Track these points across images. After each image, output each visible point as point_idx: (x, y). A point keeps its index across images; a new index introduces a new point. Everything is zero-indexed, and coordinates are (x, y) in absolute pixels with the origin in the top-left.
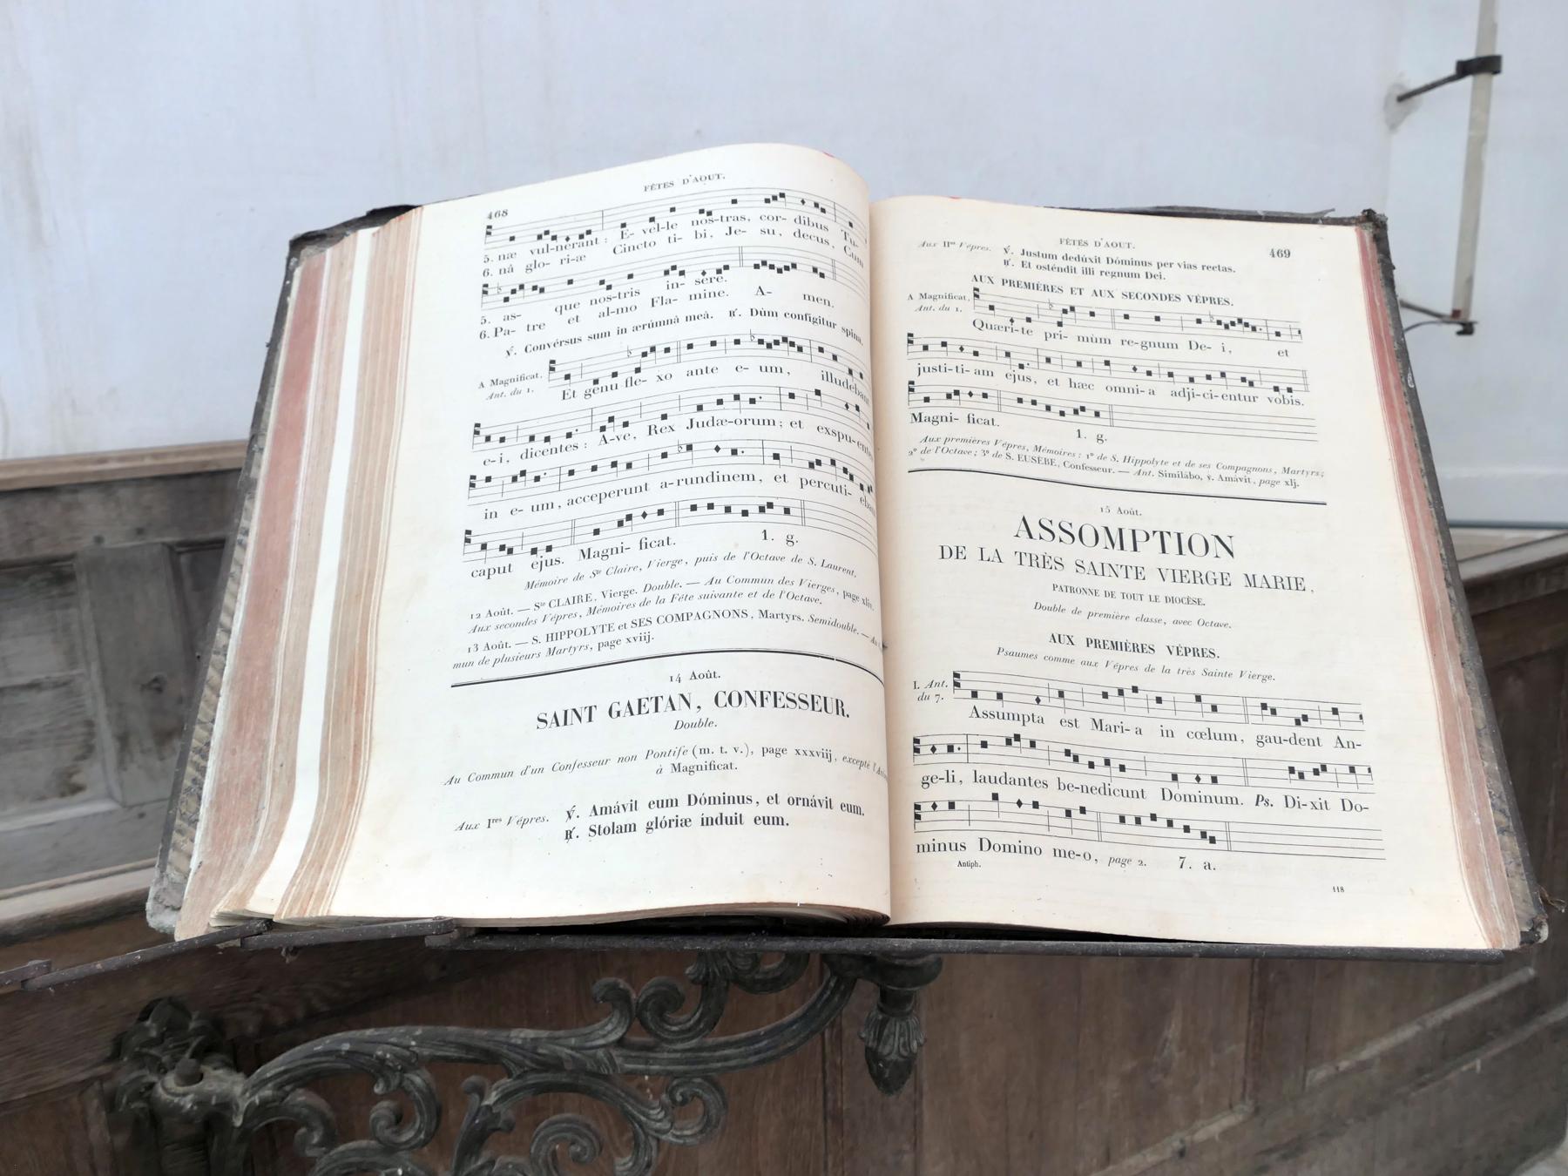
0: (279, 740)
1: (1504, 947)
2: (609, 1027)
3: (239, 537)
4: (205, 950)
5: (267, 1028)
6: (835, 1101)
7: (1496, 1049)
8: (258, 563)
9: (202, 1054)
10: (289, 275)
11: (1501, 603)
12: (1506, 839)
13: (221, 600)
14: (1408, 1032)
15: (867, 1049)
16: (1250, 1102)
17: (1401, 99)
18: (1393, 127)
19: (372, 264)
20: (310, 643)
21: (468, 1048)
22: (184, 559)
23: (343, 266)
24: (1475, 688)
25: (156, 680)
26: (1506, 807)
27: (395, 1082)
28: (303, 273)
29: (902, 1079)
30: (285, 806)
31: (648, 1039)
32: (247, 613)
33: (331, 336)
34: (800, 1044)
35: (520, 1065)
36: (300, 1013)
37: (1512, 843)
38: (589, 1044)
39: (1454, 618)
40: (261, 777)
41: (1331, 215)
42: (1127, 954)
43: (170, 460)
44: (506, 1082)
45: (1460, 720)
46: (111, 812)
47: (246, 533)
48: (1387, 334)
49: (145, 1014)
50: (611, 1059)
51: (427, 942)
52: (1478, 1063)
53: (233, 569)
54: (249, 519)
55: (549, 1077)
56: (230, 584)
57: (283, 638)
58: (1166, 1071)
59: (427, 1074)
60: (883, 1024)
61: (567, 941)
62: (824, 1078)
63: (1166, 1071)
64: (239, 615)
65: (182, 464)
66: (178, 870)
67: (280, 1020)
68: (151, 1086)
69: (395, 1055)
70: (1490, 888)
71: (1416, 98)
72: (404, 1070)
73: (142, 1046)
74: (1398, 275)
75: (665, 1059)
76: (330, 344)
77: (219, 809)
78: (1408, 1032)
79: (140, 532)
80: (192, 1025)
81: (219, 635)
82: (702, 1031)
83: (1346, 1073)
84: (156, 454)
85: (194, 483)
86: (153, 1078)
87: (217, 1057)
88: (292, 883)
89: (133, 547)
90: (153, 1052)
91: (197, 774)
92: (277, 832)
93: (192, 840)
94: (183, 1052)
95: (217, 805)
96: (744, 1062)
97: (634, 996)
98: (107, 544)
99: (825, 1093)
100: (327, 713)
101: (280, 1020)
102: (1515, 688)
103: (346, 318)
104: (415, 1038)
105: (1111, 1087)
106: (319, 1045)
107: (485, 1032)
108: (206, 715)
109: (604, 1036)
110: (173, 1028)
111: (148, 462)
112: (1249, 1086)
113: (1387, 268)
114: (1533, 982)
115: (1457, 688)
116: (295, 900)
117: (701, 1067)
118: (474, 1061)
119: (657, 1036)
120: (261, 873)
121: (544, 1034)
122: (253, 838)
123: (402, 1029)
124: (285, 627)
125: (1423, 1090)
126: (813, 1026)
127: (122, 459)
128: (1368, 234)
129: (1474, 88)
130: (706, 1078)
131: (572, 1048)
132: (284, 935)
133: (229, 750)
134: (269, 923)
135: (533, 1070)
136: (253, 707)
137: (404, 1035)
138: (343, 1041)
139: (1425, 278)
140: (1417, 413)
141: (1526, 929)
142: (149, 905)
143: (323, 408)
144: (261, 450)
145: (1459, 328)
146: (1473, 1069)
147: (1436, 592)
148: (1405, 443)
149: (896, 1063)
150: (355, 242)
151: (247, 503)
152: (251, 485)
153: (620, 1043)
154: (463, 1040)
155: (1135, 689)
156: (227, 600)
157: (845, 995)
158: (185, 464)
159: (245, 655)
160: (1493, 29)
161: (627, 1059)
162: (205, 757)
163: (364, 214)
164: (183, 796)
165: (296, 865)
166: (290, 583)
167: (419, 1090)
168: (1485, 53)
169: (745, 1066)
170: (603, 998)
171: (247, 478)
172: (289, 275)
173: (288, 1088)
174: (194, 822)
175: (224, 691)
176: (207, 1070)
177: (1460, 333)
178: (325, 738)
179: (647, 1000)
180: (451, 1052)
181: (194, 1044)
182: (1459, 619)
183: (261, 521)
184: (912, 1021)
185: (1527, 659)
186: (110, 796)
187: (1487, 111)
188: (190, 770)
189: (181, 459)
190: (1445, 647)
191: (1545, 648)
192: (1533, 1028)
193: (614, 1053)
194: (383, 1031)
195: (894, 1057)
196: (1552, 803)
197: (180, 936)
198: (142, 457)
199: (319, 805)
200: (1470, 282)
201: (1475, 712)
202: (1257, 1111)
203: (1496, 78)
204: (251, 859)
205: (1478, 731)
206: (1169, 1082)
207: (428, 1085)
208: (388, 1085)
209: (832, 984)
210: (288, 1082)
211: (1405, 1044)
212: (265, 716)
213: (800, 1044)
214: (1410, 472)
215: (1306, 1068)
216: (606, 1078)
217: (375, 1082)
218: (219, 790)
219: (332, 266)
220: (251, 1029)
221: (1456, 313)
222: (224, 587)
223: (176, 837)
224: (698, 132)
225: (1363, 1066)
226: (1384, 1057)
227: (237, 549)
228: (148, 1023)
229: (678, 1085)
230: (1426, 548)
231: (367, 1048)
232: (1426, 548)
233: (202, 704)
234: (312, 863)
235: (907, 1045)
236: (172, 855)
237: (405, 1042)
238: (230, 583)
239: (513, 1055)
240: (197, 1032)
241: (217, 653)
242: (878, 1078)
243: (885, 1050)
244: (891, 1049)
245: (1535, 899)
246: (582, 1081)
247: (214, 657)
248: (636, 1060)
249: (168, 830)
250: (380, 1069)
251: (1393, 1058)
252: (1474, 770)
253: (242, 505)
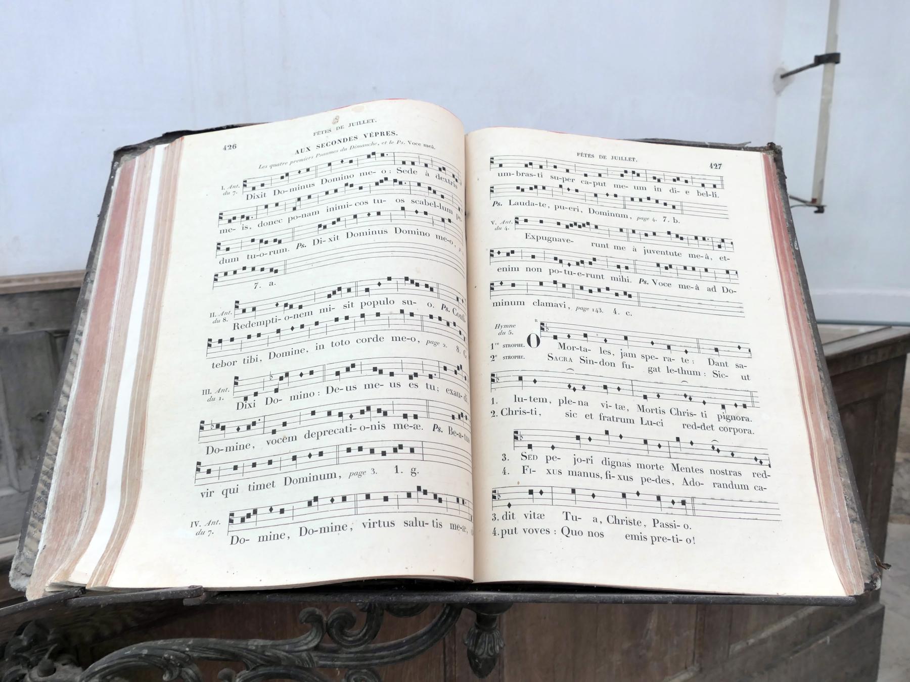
0: (96, 467)
1: (855, 594)
2: (310, 638)
3: (77, 336)
4: (43, 604)
5: (98, 638)
6: (451, 671)
7: (838, 630)
8: (88, 354)
9: (55, 656)
10: (113, 173)
11: (842, 371)
12: (855, 526)
13: (64, 377)
15: (469, 651)
16: (697, 665)
17: (783, 77)
18: (778, 92)
19: (164, 167)
20: (118, 405)
21: (222, 652)
22: (58, 341)
23: (145, 168)
24: (836, 432)
25: (40, 415)
26: (855, 506)
27: (176, 673)
28: (122, 172)
29: (490, 669)
30: (99, 511)
31: (333, 645)
32: (80, 385)
33: (137, 211)
34: (427, 648)
35: (254, 662)
36: (119, 628)
37: (858, 527)
38: (297, 649)
39: (823, 390)
40: (84, 491)
41: (749, 145)
42: (628, 602)
43: (50, 281)
44: (245, 673)
45: (827, 453)
46: (11, 496)
47: (81, 334)
48: (782, 217)
49: (20, 631)
50: (311, 659)
51: (185, 602)
52: (828, 639)
53: (72, 356)
54: (83, 325)
55: (272, 669)
56: (70, 367)
57: (101, 402)
58: (648, 648)
59: (196, 668)
60: (478, 636)
61: (277, 598)
62: (445, 658)
63: (648, 648)
64: (75, 386)
65: (57, 283)
66: (31, 550)
67: (106, 633)
68: (24, 675)
69: (176, 656)
70: (846, 556)
71: (791, 77)
72: (181, 666)
73: (17, 651)
74: (788, 182)
75: (345, 657)
76: (136, 216)
77: (57, 511)
79: (31, 324)
80: (50, 638)
81: (62, 398)
82: (366, 641)
83: (753, 645)
84: (42, 277)
86: (26, 671)
87: (66, 657)
88: (100, 563)
89: (27, 334)
90: (24, 655)
91: (45, 488)
92: (93, 527)
93: (40, 531)
94: (44, 654)
95: (57, 509)
96: (393, 659)
97: (325, 619)
98: (11, 331)
99: (445, 666)
100: (127, 450)
101: (106, 633)
102: (851, 419)
103: (146, 200)
104: (189, 646)
105: (616, 658)
106: (128, 651)
107: (231, 642)
108: (52, 450)
109: (306, 644)
110: (37, 641)
111: (37, 282)
112: (697, 656)
113: (782, 177)
115: (826, 433)
116: (100, 575)
117: (366, 663)
118: (226, 660)
119: (338, 643)
120: (80, 556)
121: (269, 643)
122: (78, 531)
123: (181, 640)
124: (102, 395)
125: (797, 655)
126: (436, 637)
127: (20, 280)
128: (771, 158)
129: (825, 71)
130: (370, 670)
131: (287, 652)
132: (92, 598)
133: (65, 473)
134: (83, 590)
135: (262, 665)
136: (82, 444)
137: (182, 644)
138: (142, 648)
139: (800, 184)
140: (800, 265)
141: (868, 582)
142: (11, 573)
143: (131, 256)
144: (92, 282)
145: (816, 209)
146: (825, 642)
147: (812, 374)
148: (793, 283)
149: (486, 660)
150: (154, 153)
151: (82, 315)
152: (86, 303)
153: (316, 648)
154: (218, 647)
155: (608, 289)
156: (68, 376)
157: (455, 618)
158: (59, 283)
159: (77, 413)
160: (836, 38)
161: (320, 657)
162: (50, 477)
164: (35, 502)
165: (104, 549)
166: (107, 366)
167: (191, 678)
168: (831, 51)
169: (394, 662)
170: (306, 621)
171: (83, 299)
172: (113, 173)
173: (109, 677)
174: (42, 519)
175: (63, 435)
176: (58, 665)
177: (816, 212)
178: (125, 467)
179: (333, 622)
180: (212, 655)
181: (52, 648)
182: (826, 391)
183: (91, 326)
184: (496, 634)
185: (856, 403)
186: (11, 485)
187: (832, 84)
188: (40, 485)
189: (57, 281)
190: (818, 407)
191: (866, 396)
192: (859, 617)
193: (313, 654)
194: (169, 642)
195: (485, 656)
196: (870, 486)
197: (31, 596)
198: (33, 279)
199: (120, 510)
200: (822, 182)
201: (835, 448)
202: (701, 670)
203: (837, 66)
204: (75, 546)
205: (838, 459)
206: (650, 654)
207: (196, 675)
208: (171, 674)
209: (447, 611)
210: (109, 674)
211: (786, 628)
212: (88, 451)
213: (427, 648)
214: (796, 301)
215: (730, 644)
216: (308, 670)
217: (163, 673)
218: (59, 499)
219: (139, 168)
220: (88, 639)
221: (814, 201)
222: (66, 368)
223: (30, 529)
224: (374, 88)
225: (763, 642)
226: (774, 636)
227: (75, 344)
228: (22, 637)
229: (352, 674)
230: (806, 347)
231: (158, 652)
232: (806, 347)
233: (50, 443)
234: (114, 548)
235: (493, 648)
236: (27, 540)
237: (183, 649)
238: (69, 365)
239: (250, 656)
240: (53, 641)
241: (60, 410)
242: (475, 669)
243: (479, 652)
244: (482, 652)
245: (873, 563)
246: (293, 671)
247: (58, 413)
248: (326, 658)
249: (25, 524)
250: (167, 665)
251: (781, 636)
252: (836, 483)
253: (79, 316)
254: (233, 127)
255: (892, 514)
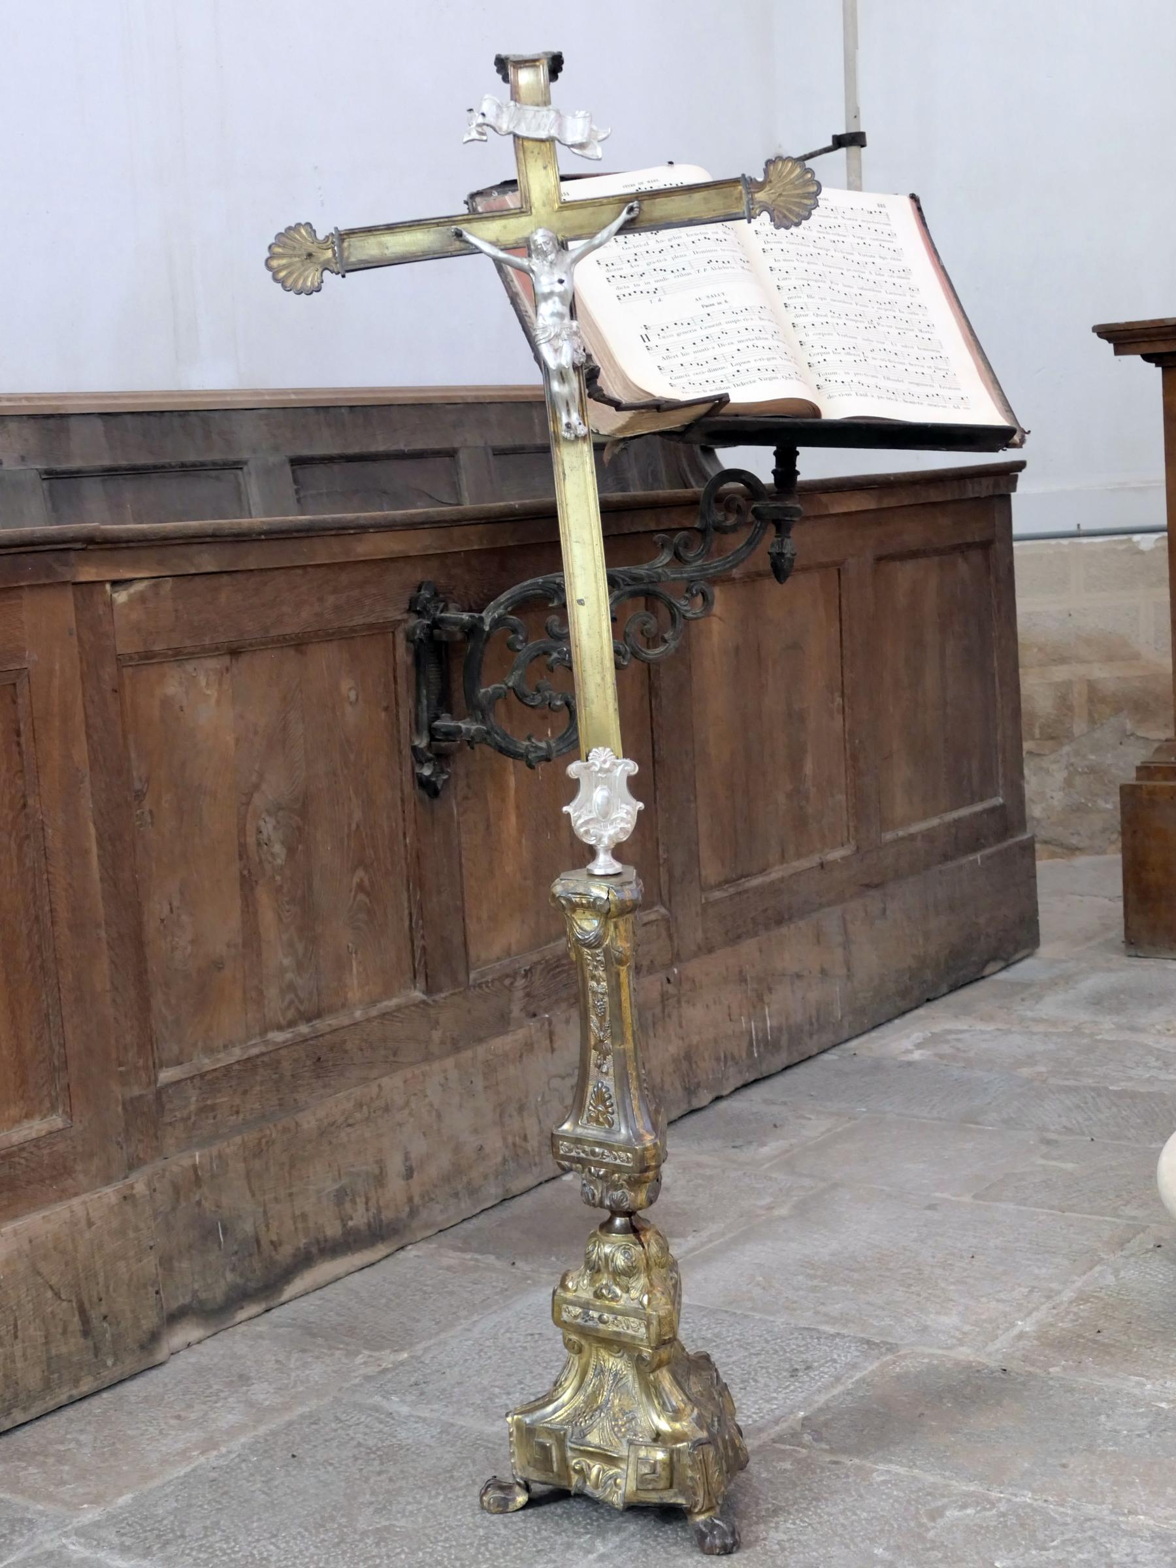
7: (988, 851)
14: (934, 822)
16: (853, 842)
78: (934, 822)
84: (28, 398)
85: (51, 421)
112: (852, 829)
114: (1003, 806)
127: (9, 400)
146: (976, 861)
161: (673, 573)
163: (498, 183)
198: (20, 399)
203: (863, 149)
211: (933, 828)
225: (912, 837)
243: (785, 551)
251: (929, 836)
254: (597, 175)
255: (1024, 734)
